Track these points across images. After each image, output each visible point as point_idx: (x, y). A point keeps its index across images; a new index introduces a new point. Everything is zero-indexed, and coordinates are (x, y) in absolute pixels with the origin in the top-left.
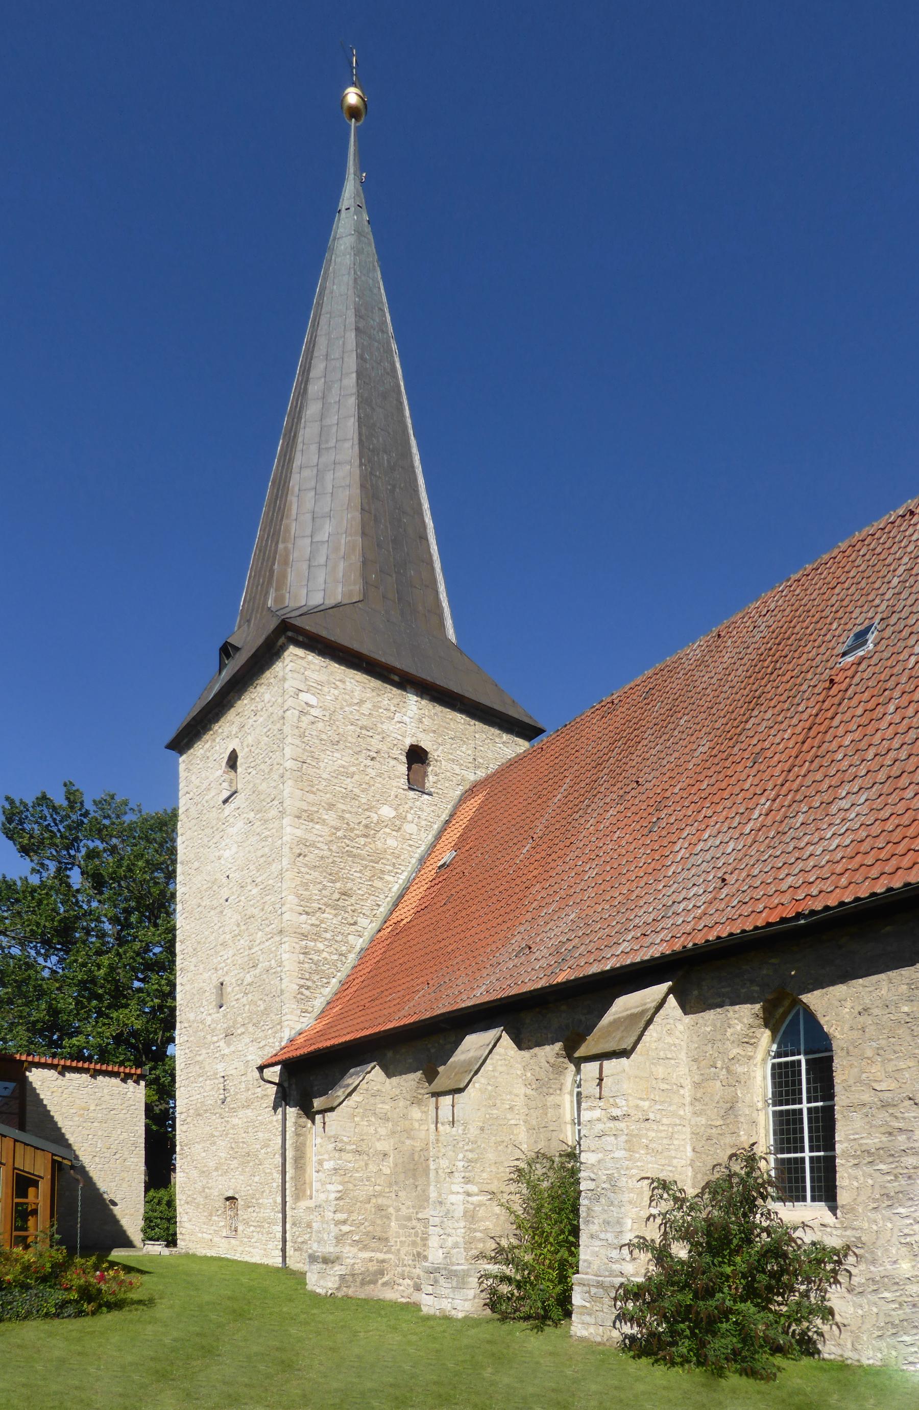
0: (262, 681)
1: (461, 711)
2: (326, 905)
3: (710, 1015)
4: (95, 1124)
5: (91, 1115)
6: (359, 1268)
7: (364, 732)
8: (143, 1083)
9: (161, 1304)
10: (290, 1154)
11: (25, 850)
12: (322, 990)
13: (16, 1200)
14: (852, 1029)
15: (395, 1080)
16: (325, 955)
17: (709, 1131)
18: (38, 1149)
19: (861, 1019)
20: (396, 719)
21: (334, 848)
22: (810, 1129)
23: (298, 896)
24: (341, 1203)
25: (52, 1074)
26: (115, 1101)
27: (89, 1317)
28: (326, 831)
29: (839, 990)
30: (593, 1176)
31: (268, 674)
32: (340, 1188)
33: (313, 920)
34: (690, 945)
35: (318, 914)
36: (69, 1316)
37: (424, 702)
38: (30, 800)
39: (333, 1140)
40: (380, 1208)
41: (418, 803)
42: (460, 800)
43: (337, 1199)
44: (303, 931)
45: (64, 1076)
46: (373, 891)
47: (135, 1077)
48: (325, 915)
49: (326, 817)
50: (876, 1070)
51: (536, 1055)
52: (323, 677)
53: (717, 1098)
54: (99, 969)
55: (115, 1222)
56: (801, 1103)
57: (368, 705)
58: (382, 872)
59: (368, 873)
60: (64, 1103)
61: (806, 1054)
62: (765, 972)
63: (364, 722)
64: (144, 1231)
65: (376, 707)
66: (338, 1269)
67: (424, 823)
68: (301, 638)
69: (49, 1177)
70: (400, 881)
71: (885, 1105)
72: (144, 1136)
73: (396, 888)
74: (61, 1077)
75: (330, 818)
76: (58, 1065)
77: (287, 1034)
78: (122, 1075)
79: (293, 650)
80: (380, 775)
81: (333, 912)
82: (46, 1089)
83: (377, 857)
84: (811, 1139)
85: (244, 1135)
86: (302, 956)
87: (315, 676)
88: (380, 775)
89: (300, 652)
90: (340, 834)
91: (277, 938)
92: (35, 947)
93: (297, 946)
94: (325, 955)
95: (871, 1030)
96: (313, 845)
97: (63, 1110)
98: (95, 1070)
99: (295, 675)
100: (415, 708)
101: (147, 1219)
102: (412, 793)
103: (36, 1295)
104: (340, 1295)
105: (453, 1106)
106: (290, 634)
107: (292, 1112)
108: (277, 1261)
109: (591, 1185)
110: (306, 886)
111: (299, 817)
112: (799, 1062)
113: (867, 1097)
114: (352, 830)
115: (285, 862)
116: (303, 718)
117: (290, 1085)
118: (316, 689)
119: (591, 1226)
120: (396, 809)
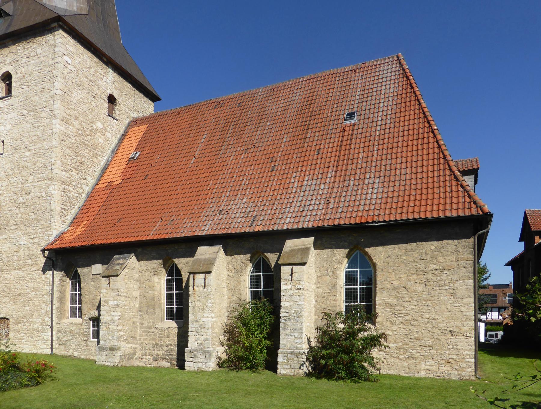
0: (35, 41)
1: (130, 83)
2: (74, 168)
3: (326, 251)
6: (127, 352)
7: (91, 83)
10: (56, 295)
12: (71, 211)
14: (384, 262)
15: (142, 263)
16: (72, 193)
17: (323, 294)
19: (388, 259)
20: (104, 80)
21: (77, 139)
22: (360, 295)
23: (62, 161)
24: (120, 321)
28: (74, 130)
29: (380, 248)
30: (287, 311)
31: (40, 38)
32: (120, 314)
33: (68, 175)
34: (326, 225)
35: (70, 172)
37: (115, 74)
39: (116, 291)
40: (134, 323)
41: (112, 123)
42: (129, 125)
43: (119, 319)
44: (63, 180)
46: (93, 164)
48: (73, 173)
49: (74, 123)
50: (393, 277)
51: (235, 258)
52: (74, 50)
53: (328, 282)
56: (357, 285)
57: (93, 70)
58: (97, 155)
59: (91, 154)
61: (360, 268)
62: (350, 238)
63: (91, 78)
65: (96, 71)
66: (119, 353)
67: (114, 134)
68: (66, 27)
70: (104, 161)
71: (395, 289)
73: (102, 164)
75: (76, 123)
77: (55, 233)
79: (61, 31)
80: (97, 106)
81: (76, 172)
83: (95, 147)
84: (360, 298)
85: (16, 284)
86: (63, 193)
87: (71, 48)
88: (97, 106)
89: (65, 34)
90: (80, 132)
91: (48, 182)
93: (61, 188)
94: (72, 193)
95: (391, 263)
96: (68, 136)
99: (62, 46)
100: (112, 76)
102: (109, 118)
104: (119, 365)
105: (205, 279)
106: (61, 23)
107: (58, 275)
108: (49, 351)
109: (287, 315)
110: (65, 156)
111: (63, 121)
112: (357, 271)
113: (389, 286)
114: (85, 131)
115: (54, 143)
116: (65, 69)
117: (57, 260)
118: (71, 55)
119: (286, 331)
120: (103, 125)
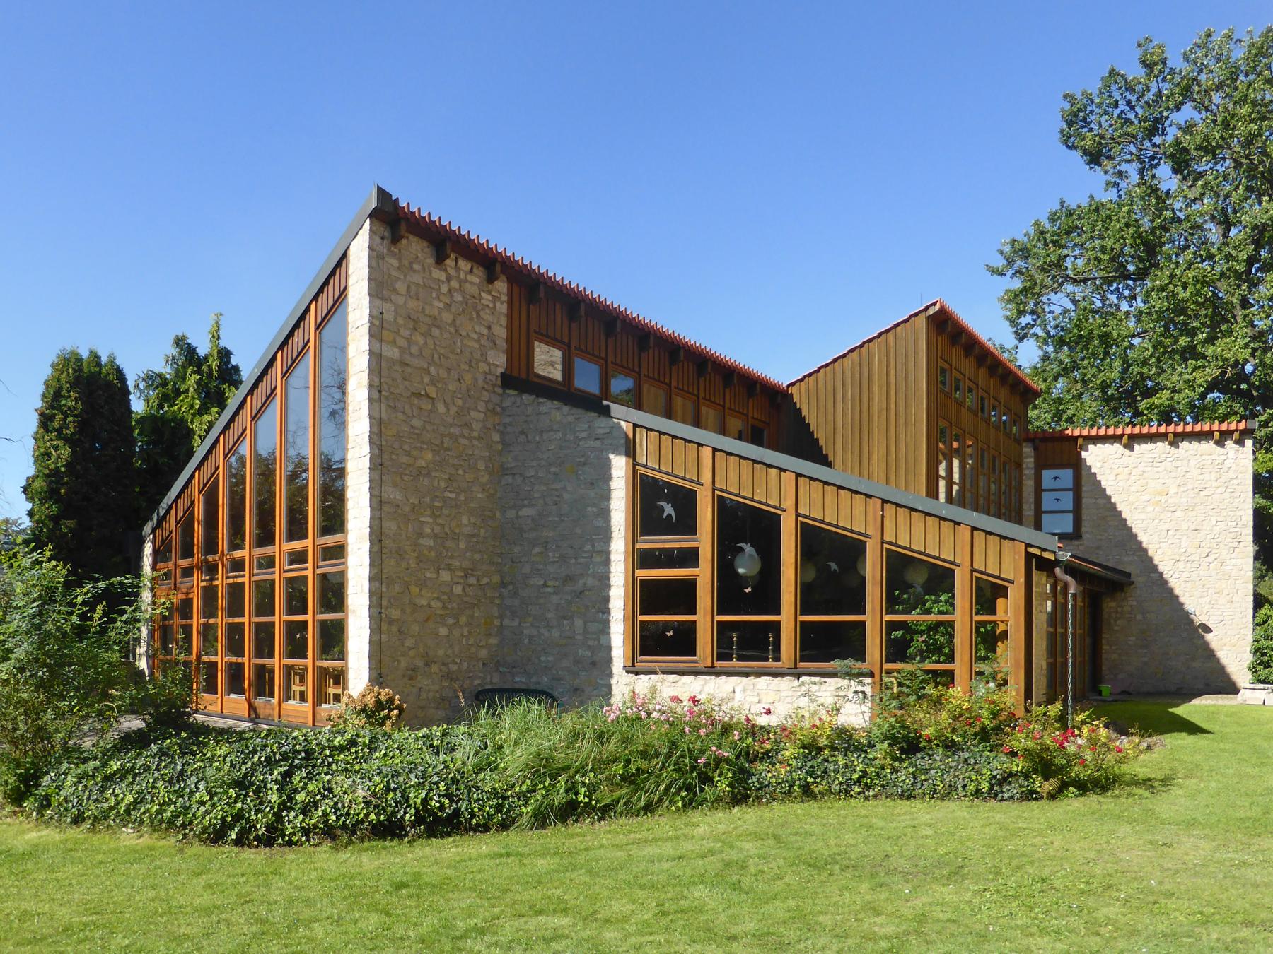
4: (1178, 513)
5: (1170, 501)
8: (1249, 443)
9: (1181, 787)
11: (1094, 158)
13: (977, 618)
18: (1005, 538)
25: (1117, 448)
26: (1207, 476)
27: (1044, 802)
36: (1012, 797)
38: (1094, 87)
45: (1132, 450)
47: (1236, 435)
54: (1185, 288)
55: (1210, 655)
60: (1132, 489)
64: (1253, 669)
69: (1022, 580)
72: (1251, 524)
74: (1127, 452)
76: (1123, 435)
78: (1217, 435)
82: (1108, 471)
92: (1117, 289)
97: (1131, 499)
98: (1176, 434)
101: (1258, 651)
103: (966, 760)
